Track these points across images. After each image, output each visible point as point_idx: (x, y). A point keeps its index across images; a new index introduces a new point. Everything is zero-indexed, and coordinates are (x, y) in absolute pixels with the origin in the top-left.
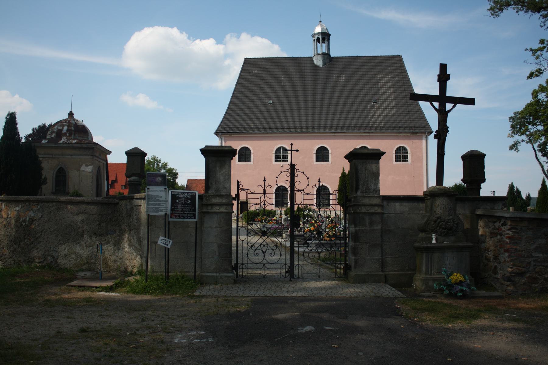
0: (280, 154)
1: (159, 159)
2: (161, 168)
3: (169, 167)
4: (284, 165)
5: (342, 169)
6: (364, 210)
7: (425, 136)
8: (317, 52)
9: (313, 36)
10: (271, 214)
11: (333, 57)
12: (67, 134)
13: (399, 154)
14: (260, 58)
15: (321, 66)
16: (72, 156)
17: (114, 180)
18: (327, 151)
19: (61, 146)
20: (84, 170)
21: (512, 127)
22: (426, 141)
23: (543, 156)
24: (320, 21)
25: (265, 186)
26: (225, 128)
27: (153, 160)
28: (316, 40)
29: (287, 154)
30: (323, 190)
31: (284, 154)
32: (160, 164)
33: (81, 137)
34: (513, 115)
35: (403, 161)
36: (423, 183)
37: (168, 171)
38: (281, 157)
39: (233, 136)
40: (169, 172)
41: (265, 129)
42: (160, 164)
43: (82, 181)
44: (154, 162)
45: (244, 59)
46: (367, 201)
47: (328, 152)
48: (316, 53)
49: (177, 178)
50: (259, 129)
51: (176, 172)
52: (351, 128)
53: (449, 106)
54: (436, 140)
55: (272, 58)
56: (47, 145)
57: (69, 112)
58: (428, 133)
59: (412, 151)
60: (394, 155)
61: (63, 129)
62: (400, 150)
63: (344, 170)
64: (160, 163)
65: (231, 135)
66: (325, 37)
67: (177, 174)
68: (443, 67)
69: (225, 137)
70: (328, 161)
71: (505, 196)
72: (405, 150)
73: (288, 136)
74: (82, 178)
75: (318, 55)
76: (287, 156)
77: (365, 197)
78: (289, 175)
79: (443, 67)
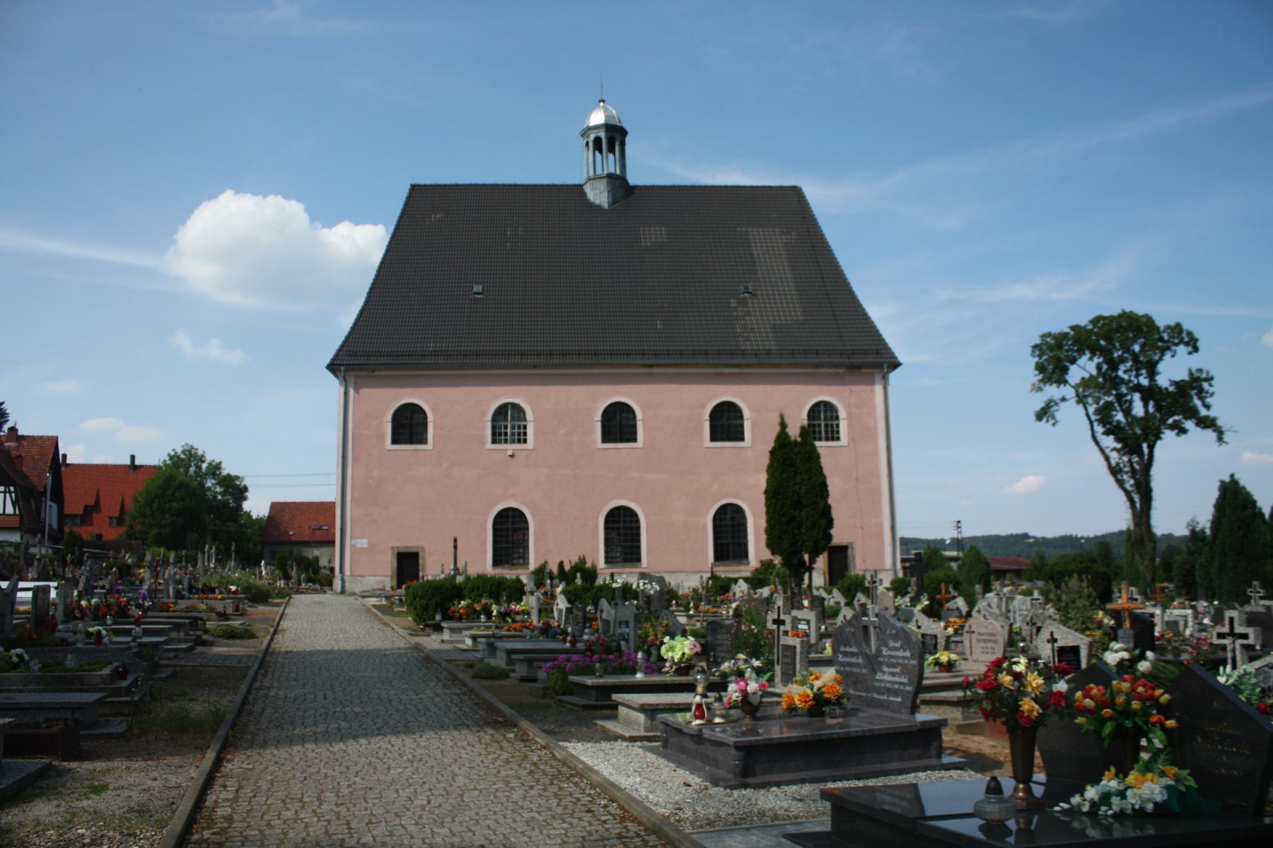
0: (505, 423)
1: (200, 452)
2: (206, 474)
3: (225, 473)
4: (516, 453)
5: (778, 419)
7: (882, 375)
8: (595, 172)
9: (585, 133)
10: (504, 590)
11: (635, 187)
13: (816, 422)
14: (451, 185)
15: (606, 205)
17: (91, 506)
18: (631, 415)
21: (1040, 368)
22: (885, 388)
23: (1107, 433)
24: (600, 99)
26: (355, 354)
27: (185, 455)
28: (591, 144)
29: (525, 423)
30: (622, 519)
31: (516, 423)
32: (204, 466)
34: (1038, 341)
35: (827, 439)
36: (880, 495)
37: (224, 481)
39: (377, 373)
40: (224, 483)
41: (464, 355)
42: (204, 466)
44: (189, 460)
45: (409, 187)
47: (635, 417)
48: (591, 173)
49: (245, 499)
50: (448, 355)
51: (243, 485)
52: (694, 354)
55: (480, 185)
58: (888, 367)
62: (819, 412)
63: (783, 425)
64: (204, 462)
65: (373, 371)
66: (613, 137)
67: (246, 489)
69: (356, 377)
70: (635, 440)
71: (1123, 527)
72: (831, 411)
76: (525, 427)
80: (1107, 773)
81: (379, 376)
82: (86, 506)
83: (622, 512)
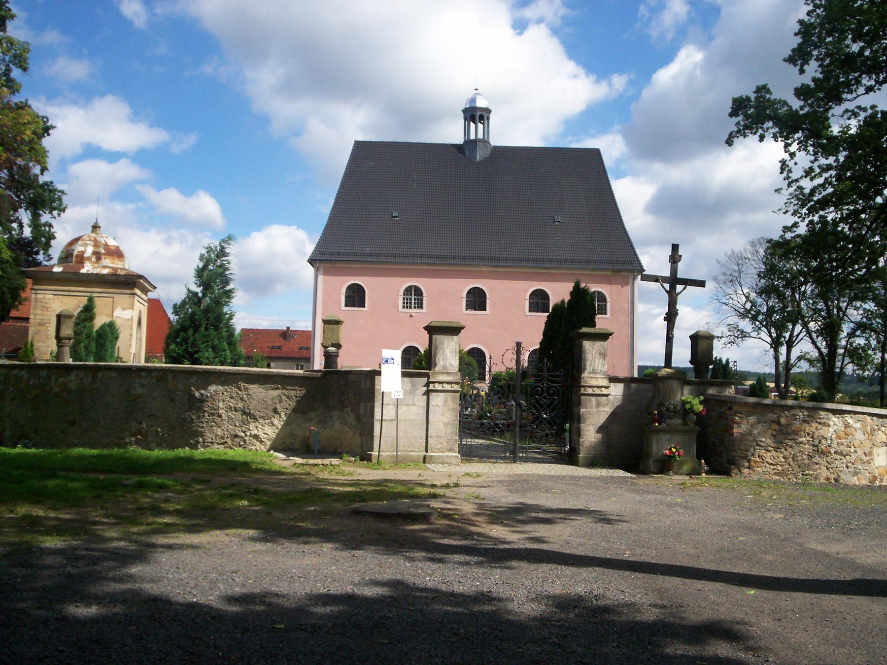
6: (590, 391)
7: (633, 276)
20: (118, 315)
25: (490, 364)
33: (113, 263)
38: (413, 301)
46: (594, 382)
53: (679, 288)
54: (666, 322)
61: (86, 250)
68: (675, 248)
69: (324, 267)
77: (592, 378)
78: (515, 353)
79: (675, 248)
80: (431, 506)
81: (338, 267)
83: (476, 351)
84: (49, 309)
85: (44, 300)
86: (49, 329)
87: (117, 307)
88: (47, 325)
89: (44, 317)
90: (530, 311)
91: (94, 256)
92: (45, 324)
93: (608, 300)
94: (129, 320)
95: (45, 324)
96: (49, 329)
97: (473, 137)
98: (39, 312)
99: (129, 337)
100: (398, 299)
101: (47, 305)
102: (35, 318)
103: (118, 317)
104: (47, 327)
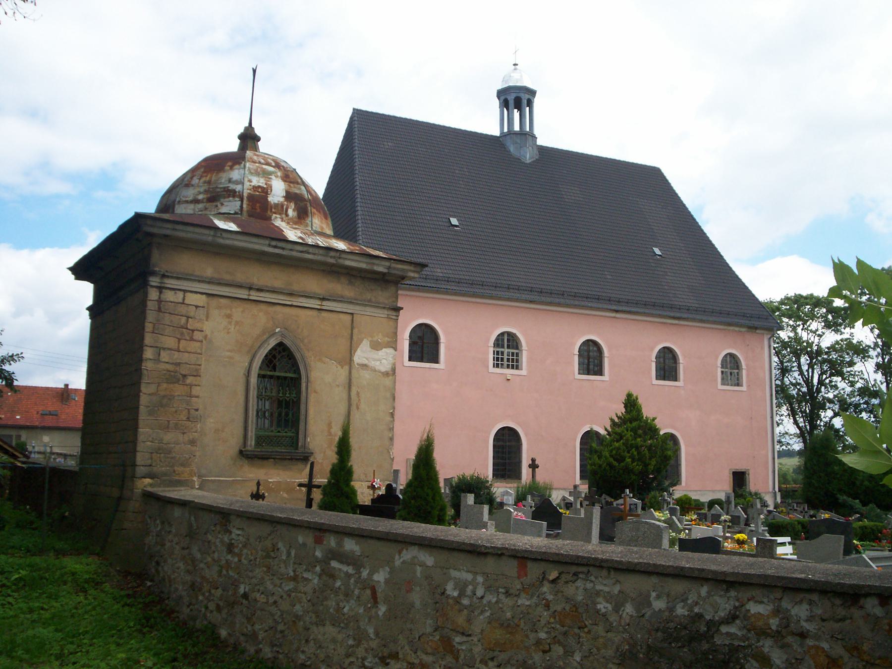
0: (502, 350)
12: (291, 212)
16: (324, 303)
19: (294, 254)
20: (365, 362)
31: (511, 351)
38: (505, 357)
43: (358, 408)
56: (236, 243)
57: (241, 130)
59: (747, 365)
60: (719, 370)
73: (534, 309)
74: (358, 394)
75: (519, 135)
82: (883, 268)
84: (197, 335)
85: (182, 309)
86: (196, 391)
87: (361, 341)
88: (190, 380)
89: (185, 357)
90: (410, 359)
91: (292, 205)
92: (185, 376)
93: (744, 366)
94: (386, 374)
95: (185, 376)
96: (196, 391)
97: (517, 128)
98: (169, 342)
99: (389, 418)
100: (488, 354)
101: (192, 324)
102: (157, 360)
103: (364, 366)
104: (191, 386)
